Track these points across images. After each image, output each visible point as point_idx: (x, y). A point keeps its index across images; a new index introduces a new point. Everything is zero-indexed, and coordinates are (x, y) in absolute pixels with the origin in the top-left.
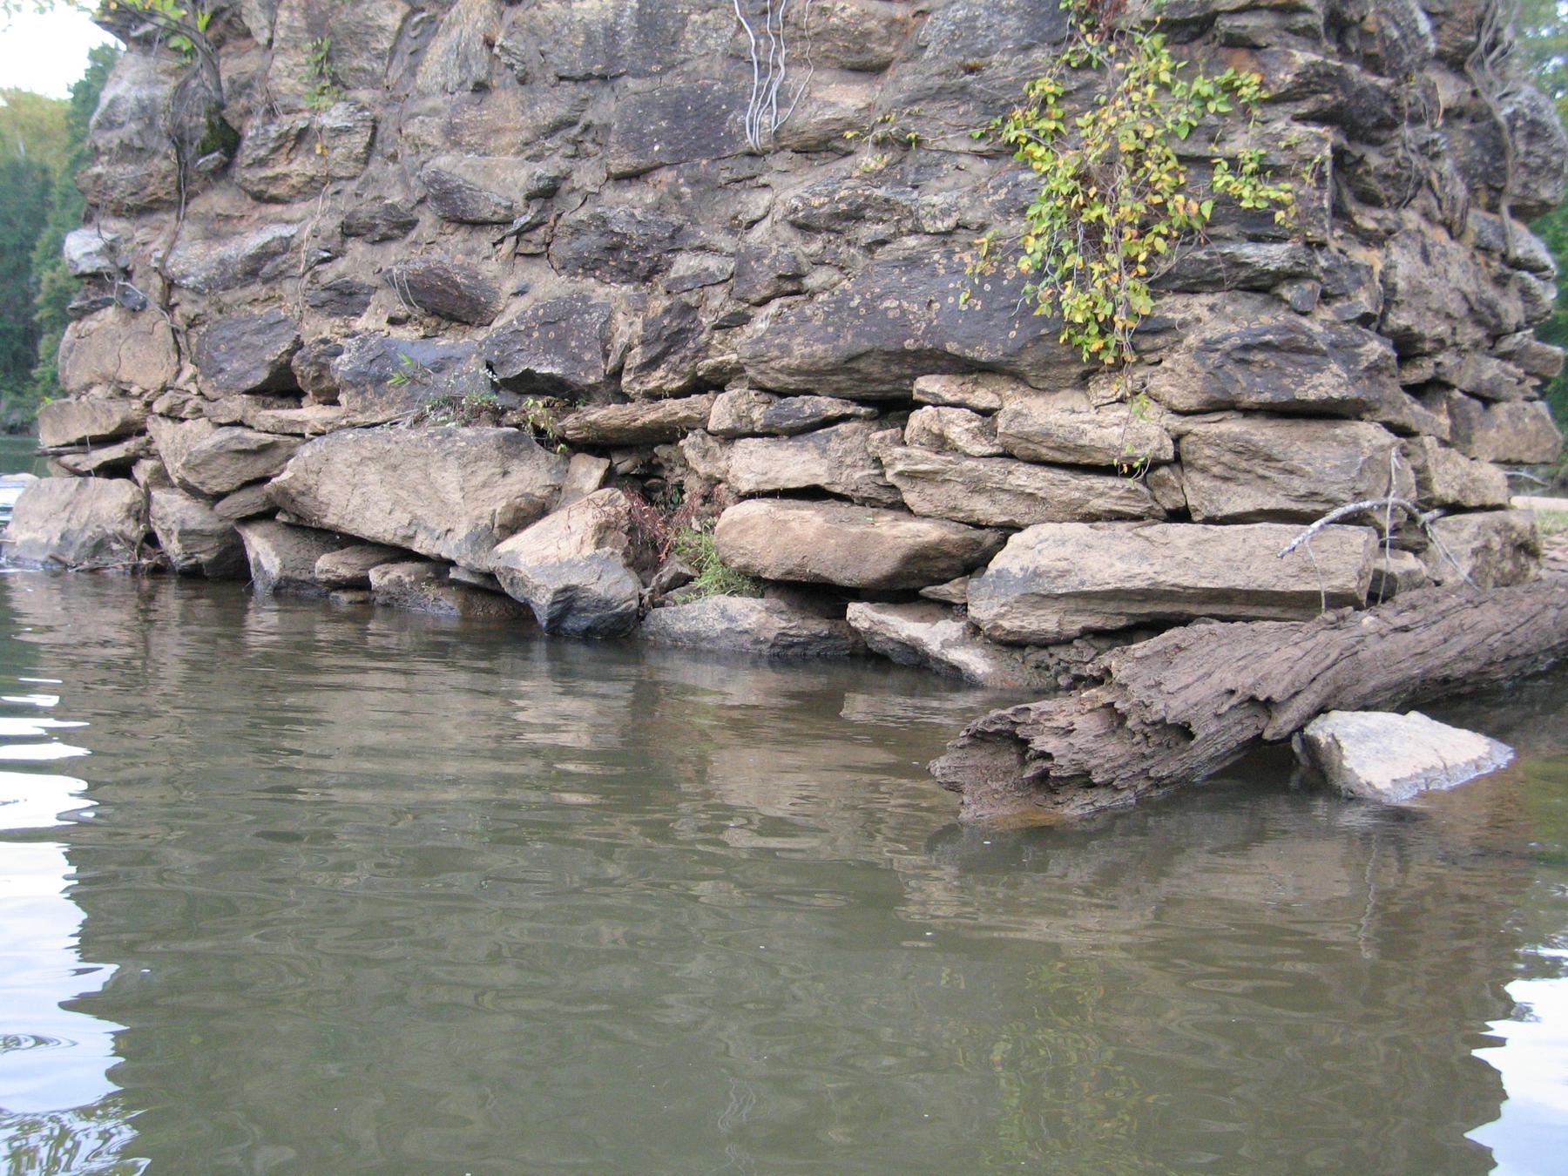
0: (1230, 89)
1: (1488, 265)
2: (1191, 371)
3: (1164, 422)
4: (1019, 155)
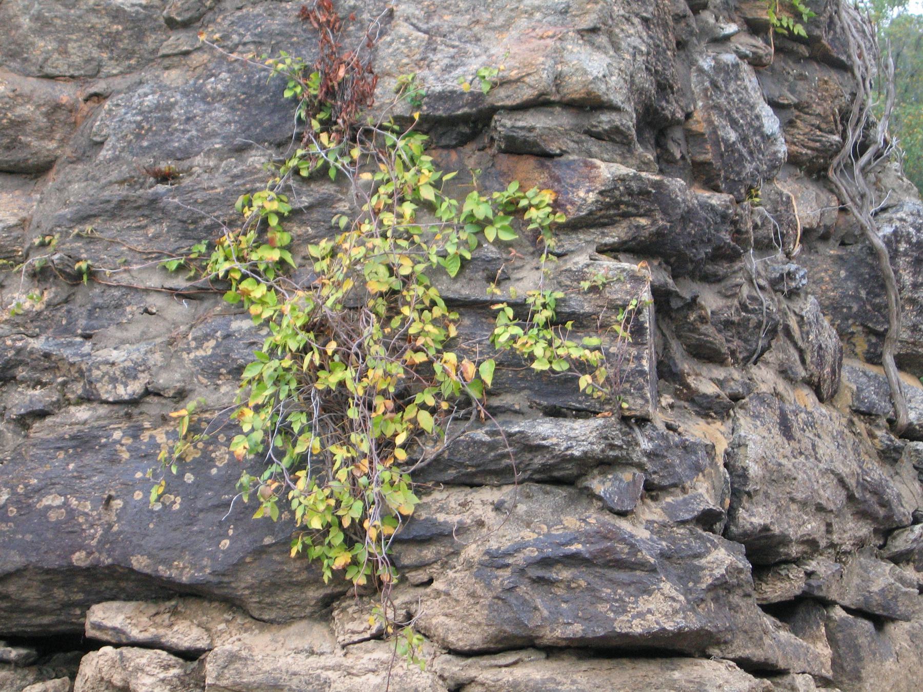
0: (514, 211)
1: (872, 436)
2: (472, 595)
3: (437, 666)
4: (230, 295)
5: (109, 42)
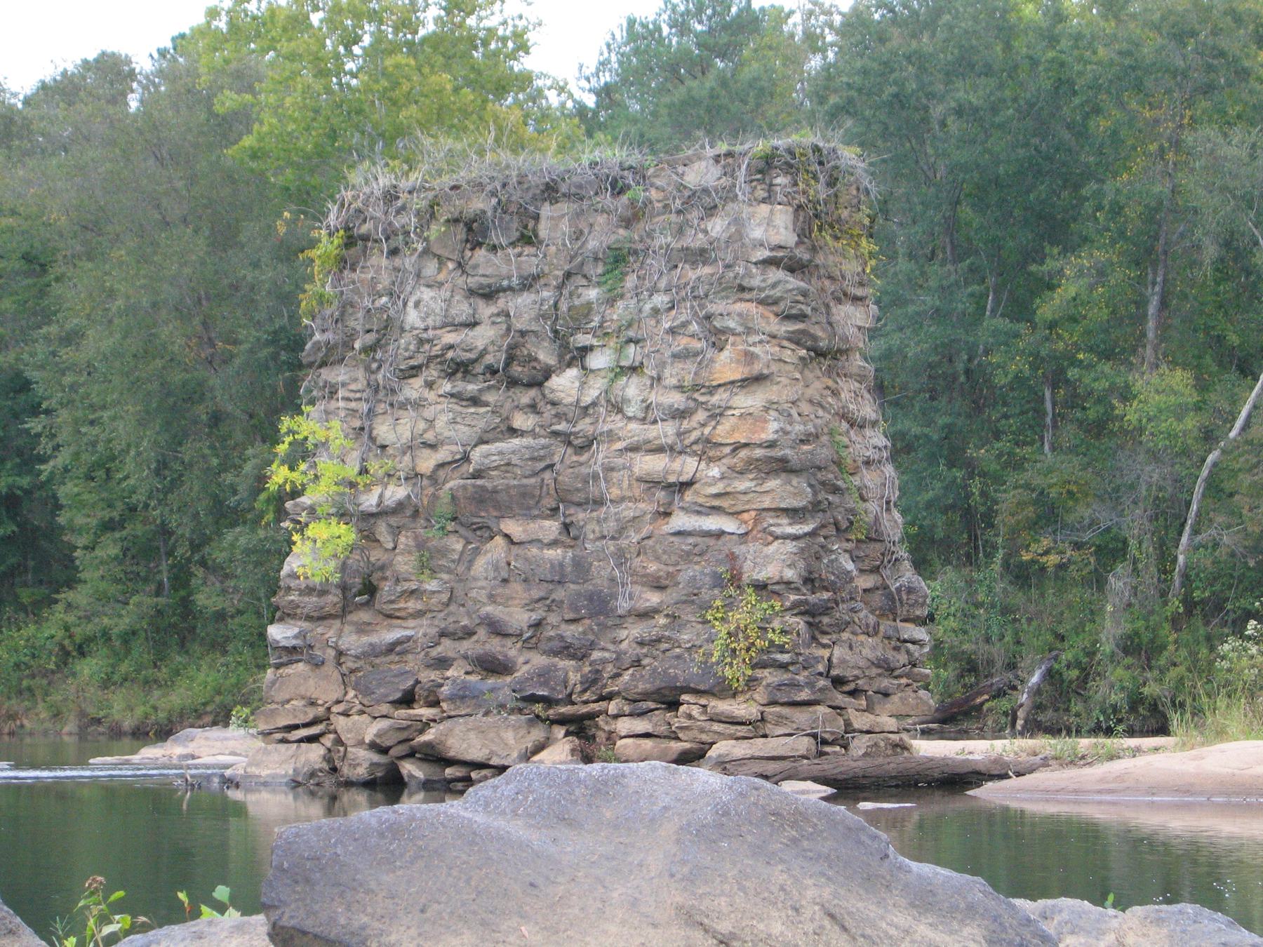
0: (772, 607)
5: (681, 557)
